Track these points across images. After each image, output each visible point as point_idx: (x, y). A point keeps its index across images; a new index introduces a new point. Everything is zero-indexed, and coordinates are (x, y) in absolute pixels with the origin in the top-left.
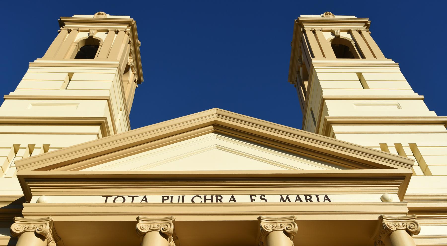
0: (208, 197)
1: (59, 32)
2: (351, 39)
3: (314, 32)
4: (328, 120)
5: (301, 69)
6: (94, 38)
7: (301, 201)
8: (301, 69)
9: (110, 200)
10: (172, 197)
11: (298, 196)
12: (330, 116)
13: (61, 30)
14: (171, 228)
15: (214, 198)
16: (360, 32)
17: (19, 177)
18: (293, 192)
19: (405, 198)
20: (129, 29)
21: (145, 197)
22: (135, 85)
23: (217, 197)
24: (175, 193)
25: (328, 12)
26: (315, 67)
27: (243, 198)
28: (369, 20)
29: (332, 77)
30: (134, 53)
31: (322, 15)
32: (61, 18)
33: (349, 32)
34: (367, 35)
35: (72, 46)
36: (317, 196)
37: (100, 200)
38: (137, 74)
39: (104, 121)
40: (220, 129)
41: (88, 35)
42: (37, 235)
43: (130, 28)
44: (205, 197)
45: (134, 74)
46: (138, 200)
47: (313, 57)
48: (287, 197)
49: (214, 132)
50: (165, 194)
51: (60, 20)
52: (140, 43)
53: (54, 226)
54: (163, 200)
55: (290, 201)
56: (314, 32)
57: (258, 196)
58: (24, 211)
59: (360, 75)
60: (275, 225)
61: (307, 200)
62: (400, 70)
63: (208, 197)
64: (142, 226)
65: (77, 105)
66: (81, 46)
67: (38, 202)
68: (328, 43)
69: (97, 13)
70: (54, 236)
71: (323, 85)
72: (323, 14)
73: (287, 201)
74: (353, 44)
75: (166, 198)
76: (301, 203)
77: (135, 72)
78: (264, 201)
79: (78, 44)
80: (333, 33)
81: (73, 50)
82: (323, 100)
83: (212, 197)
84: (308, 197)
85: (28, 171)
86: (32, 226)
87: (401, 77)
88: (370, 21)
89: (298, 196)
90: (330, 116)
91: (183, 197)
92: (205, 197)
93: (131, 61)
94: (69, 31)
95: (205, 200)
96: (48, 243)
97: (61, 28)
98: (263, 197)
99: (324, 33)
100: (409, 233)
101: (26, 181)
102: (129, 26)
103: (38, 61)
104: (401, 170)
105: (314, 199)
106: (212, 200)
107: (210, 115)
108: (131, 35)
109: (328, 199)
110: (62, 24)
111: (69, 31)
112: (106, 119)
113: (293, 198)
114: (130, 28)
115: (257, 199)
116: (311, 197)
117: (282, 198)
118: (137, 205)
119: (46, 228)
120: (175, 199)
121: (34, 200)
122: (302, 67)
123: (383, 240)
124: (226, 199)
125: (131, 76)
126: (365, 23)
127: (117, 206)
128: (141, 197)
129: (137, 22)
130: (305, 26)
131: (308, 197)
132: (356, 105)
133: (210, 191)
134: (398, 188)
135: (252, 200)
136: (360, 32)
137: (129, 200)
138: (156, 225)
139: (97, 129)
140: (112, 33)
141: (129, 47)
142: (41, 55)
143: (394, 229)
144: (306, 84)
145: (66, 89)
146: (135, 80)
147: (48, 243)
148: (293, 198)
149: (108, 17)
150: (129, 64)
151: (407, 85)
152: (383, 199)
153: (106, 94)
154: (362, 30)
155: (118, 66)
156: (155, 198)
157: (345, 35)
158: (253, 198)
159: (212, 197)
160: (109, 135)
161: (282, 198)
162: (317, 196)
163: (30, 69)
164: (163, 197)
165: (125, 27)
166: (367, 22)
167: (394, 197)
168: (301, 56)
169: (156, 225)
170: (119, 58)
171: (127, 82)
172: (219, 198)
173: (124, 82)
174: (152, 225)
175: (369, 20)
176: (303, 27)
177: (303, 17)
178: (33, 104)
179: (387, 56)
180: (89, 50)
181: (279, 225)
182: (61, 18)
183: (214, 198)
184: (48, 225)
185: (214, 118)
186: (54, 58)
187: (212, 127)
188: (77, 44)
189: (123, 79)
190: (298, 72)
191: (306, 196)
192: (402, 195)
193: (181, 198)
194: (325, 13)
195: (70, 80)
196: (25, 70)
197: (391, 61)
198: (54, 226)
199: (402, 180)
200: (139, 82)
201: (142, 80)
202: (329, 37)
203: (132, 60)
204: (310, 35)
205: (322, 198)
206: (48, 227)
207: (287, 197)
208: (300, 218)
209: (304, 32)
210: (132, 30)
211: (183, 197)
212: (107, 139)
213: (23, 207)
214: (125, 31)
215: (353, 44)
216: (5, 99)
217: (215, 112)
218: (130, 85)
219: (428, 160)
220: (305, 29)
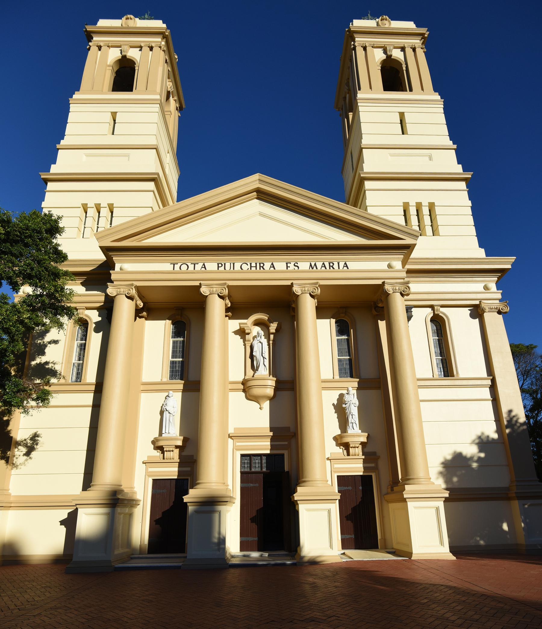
0: (254, 264)
1: (89, 49)
2: (403, 60)
3: (365, 48)
4: (362, 176)
5: (348, 95)
6: (128, 57)
7: (326, 268)
8: (348, 95)
9: (177, 267)
10: (225, 264)
11: (323, 264)
12: (365, 171)
13: (90, 46)
14: (226, 292)
15: (258, 265)
16: (414, 50)
17: (101, 247)
18: (320, 260)
19: (409, 261)
20: (163, 43)
21: (204, 264)
22: (177, 114)
23: (260, 264)
24: (227, 260)
25: (384, 17)
26: (359, 104)
27: (280, 266)
28: (427, 31)
29: (376, 115)
30: (172, 75)
31: (377, 20)
32: (86, 27)
33: (403, 49)
34: (421, 54)
35: (107, 71)
36: (338, 263)
37: (168, 267)
38: (178, 101)
39: (156, 176)
40: (263, 196)
41: (121, 53)
42: (128, 297)
43: (165, 40)
44: (251, 264)
45: (175, 100)
46: (199, 267)
47: (360, 89)
48: (315, 265)
49: (258, 198)
50: (219, 262)
51: (86, 31)
52: (176, 57)
53: (139, 289)
54: (218, 267)
55: (317, 268)
56: (365, 48)
57: (293, 263)
58: (113, 277)
59: (402, 115)
60: (303, 289)
61: (330, 266)
62: (444, 109)
63: (254, 264)
64: (204, 290)
65: (128, 156)
66: (115, 70)
67: (121, 269)
68: (378, 66)
69: (125, 17)
70: (139, 296)
71: (364, 128)
72: (378, 18)
73: (315, 268)
74: (404, 69)
75: (220, 265)
76: (326, 270)
77: (176, 98)
78: (296, 268)
79: (112, 67)
80: (385, 52)
81: (108, 78)
82: (361, 149)
83: (256, 264)
84: (331, 264)
85: (108, 243)
86: (122, 290)
87: (442, 119)
88: (428, 33)
89: (323, 264)
90: (365, 171)
91: (234, 264)
92: (251, 264)
93: (170, 85)
94: (100, 48)
95: (251, 267)
96: (136, 301)
97: (90, 44)
98: (296, 264)
99: (374, 49)
100: (402, 295)
101: (106, 250)
102: (164, 38)
103: (76, 96)
104: (408, 241)
105: (336, 266)
106: (256, 267)
107: (253, 181)
108: (167, 52)
109: (347, 266)
110: (89, 37)
111: (100, 48)
112: (158, 174)
113: (319, 265)
114: (165, 40)
115: (292, 266)
116: (333, 264)
117: (311, 265)
118: (198, 272)
119: (133, 292)
120: (228, 265)
121: (117, 267)
122: (348, 93)
123: (383, 299)
124: (267, 266)
125: (173, 104)
126: (422, 35)
127: (183, 273)
128: (201, 265)
129: (171, 31)
130: (356, 39)
131: (331, 264)
132: (392, 155)
133: (255, 259)
134: (403, 256)
135: (287, 267)
136: (414, 50)
137: (191, 267)
138: (215, 289)
139: (151, 185)
140: (146, 49)
141: (167, 68)
142: (77, 88)
143: (391, 292)
144: (351, 115)
145: (113, 134)
146: (177, 108)
147: (136, 301)
148: (319, 265)
149: (138, 25)
150: (169, 89)
151: (444, 130)
152: (389, 266)
153: (152, 141)
154: (417, 46)
155: (159, 102)
156: (212, 266)
157: (397, 54)
158: (289, 265)
159: (256, 264)
160: (169, 205)
161: (311, 265)
162: (338, 263)
163: (72, 107)
164: (218, 264)
165: (158, 39)
166: (424, 34)
167: (397, 264)
168: (349, 79)
169: (215, 289)
170: (158, 90)
171: (169, 113)
172: (262, 265)
173: (166, 113)
174: (211, 289)
175: (427, 31)
176: (354, 42)
177: (357, 23)
178: (87, 155)
179: (436, 89)
180: (124, 77)
181: (306, 289)
182: (86, 27)
183: (258, 265)
184: (134, 289)
185: (257, 185)
186: (92, 90)
187: (255, 193)
188: (111, 68)
189: (166, 109)
190: (345, 98)
191: (329, 263)
192: (404, 264)
193: (232, 265)
194: (380, 18)
195: (115, 121)
196: (66, 111)
197: (437, 97)
198: (139, 289)
199: (409, 248)
200: (180, 109)
201: (184, 107)
202: (379, 56)
203: (171, 84)
204: (360, 52)
205: (342, 264)
206: (134, 291)
207: (315, 265)
208: (322, 283)
209: (354, 49)
210: (167, 42)
211: (234, 264)
212: (167, 209)
213: (111, 274)
214: (160, 47)
215: (404, 69)
216: (58, 149)
217: (258, 178)
218: (172, 116)
219: (440, 220)
220: (356, 44)
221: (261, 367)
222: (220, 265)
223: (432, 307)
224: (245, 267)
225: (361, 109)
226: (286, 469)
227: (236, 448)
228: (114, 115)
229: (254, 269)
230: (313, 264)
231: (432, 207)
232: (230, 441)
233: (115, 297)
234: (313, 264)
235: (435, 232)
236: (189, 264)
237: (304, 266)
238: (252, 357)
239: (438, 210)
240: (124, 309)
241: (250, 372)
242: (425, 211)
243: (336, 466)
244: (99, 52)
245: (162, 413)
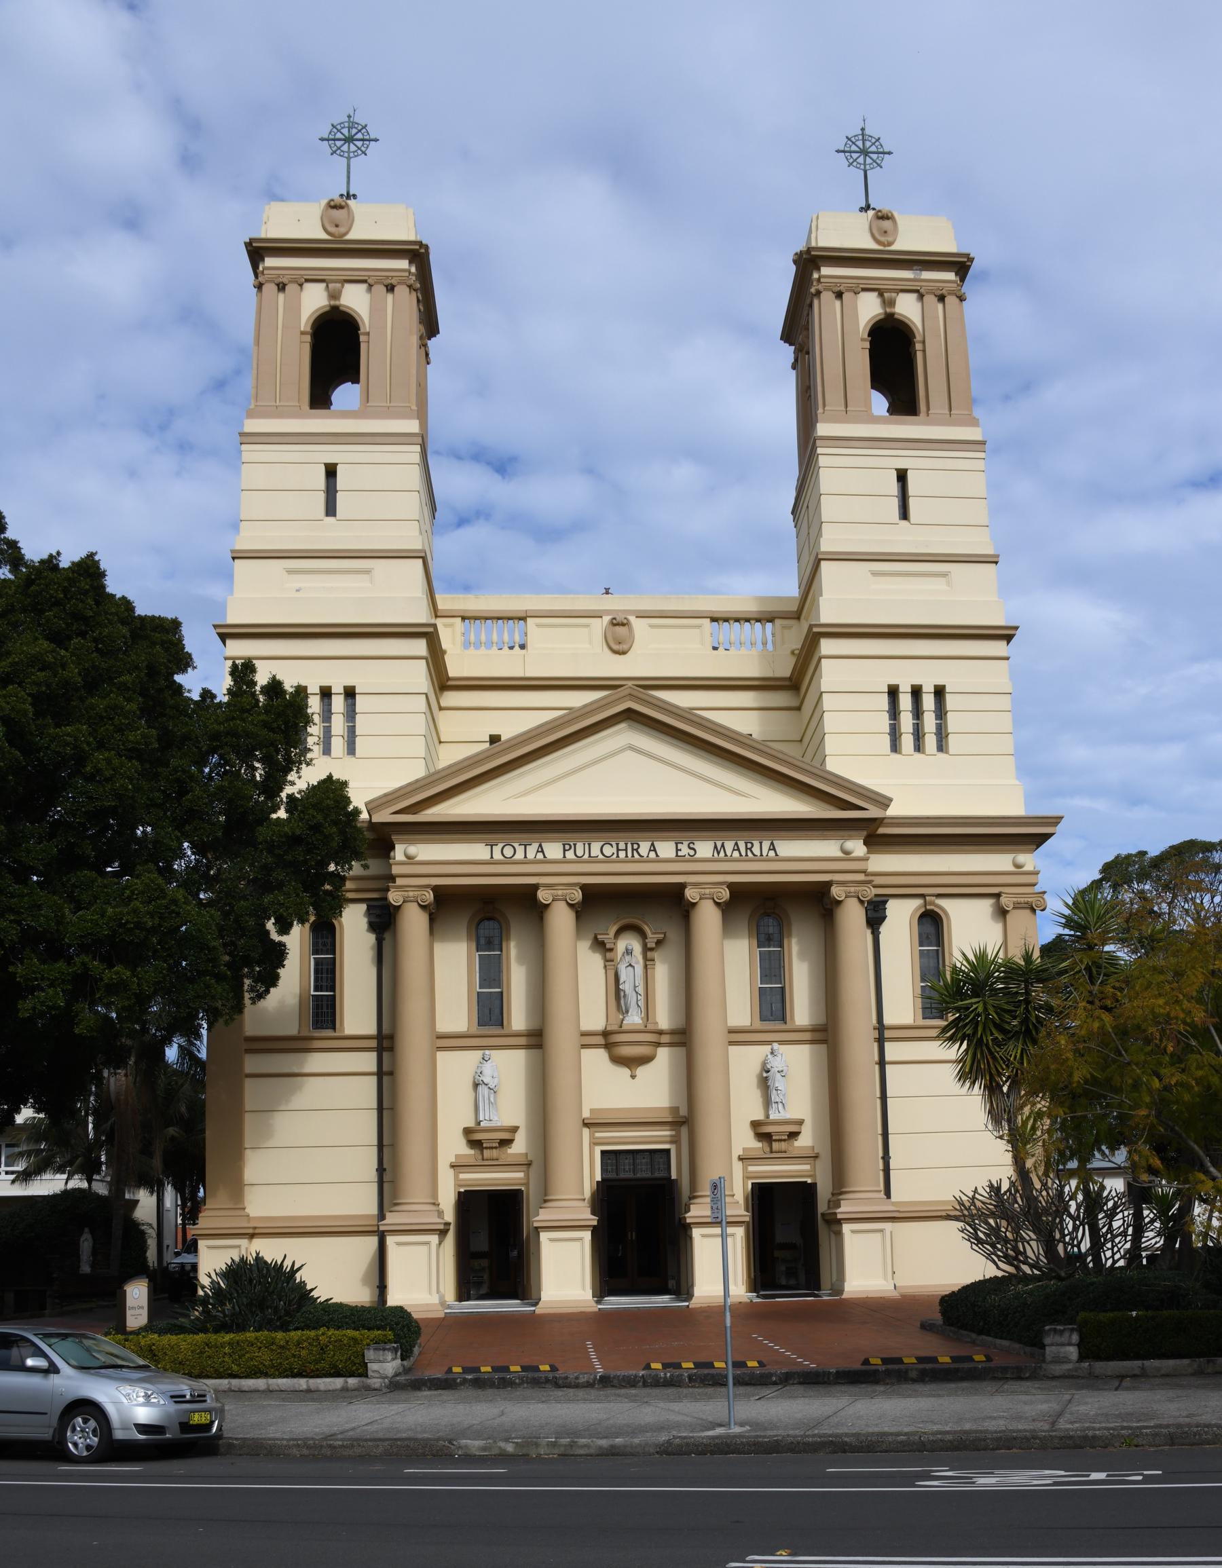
0: (622, 845)
39: (431, 630)
48: (723, 846)
54: (565, 850)
57: (686, 843)
63: (622, 845)
68: (863, 340)
78: (692, 853)
95: (618, 850)
115: (684, 850)
117: (716, 847)
124: (644, 848)
135: (677, 850)
139: (419, 647)
156: (553, 850)
158: (680, 846)
161: (716, 847)
207: (723, 846)
219: (953, 722)
221: (633, 1010)
222: (567, 847)
223: (923, 896)
224: (608, 850)
225: (822, 461)
226: (674, 1176)
227: (594, 1143)
228: (331, 472)
229: (622, 854)
230: (719, 844)
231: (939, 692)
232: (586, 1131)
233: (399, 907)
234: (719, 844)
235: (942, 747)
236: (516, 845)
237: (704, 849)
238: (618, 990)
239: (951, 702)
240: (414, 922)
241: (616, 1017)
242: (928, 702)
243: (751, 1168)
244: (281, 296)
245: (476, 1085)
